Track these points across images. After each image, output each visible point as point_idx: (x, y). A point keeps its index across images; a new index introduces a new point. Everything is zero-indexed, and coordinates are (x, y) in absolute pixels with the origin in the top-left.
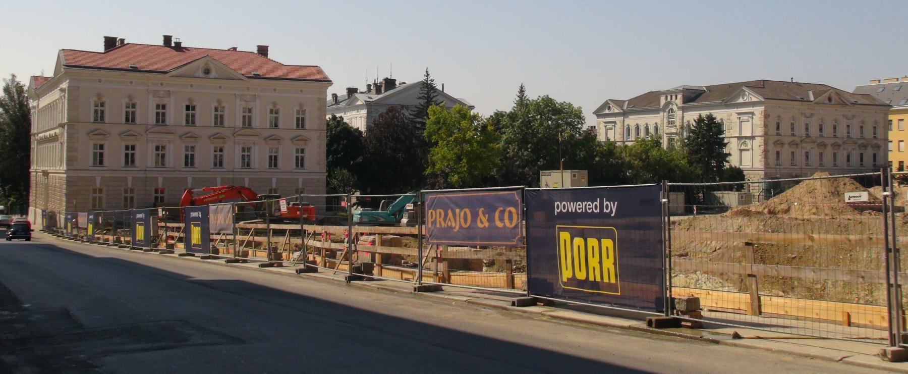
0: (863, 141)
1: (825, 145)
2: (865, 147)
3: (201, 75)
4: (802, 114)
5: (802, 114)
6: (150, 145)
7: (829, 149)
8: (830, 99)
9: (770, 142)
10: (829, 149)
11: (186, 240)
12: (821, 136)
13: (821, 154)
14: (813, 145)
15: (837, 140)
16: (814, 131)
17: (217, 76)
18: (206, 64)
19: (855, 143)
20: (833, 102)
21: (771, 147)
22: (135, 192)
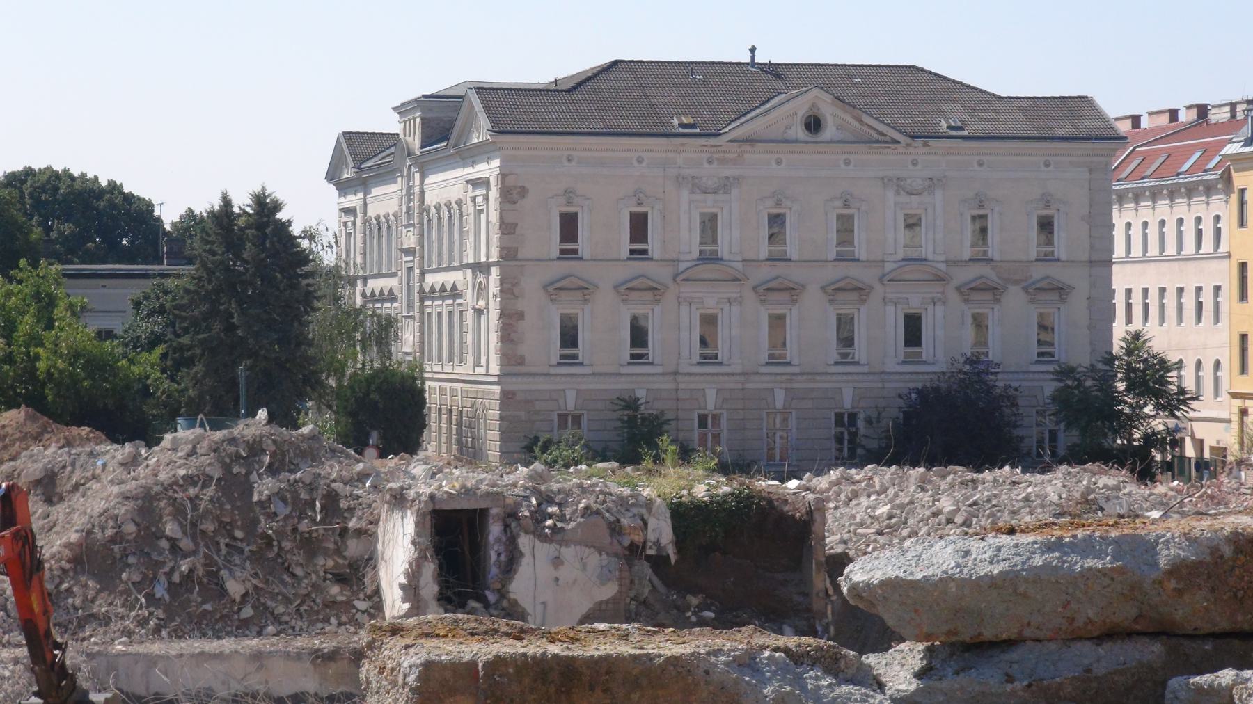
0: (986, 270)
1: (792, 291)
2: (994, 291)
3: (801, 133)
4: (680, 180)
5: (680, 180)
6: (890, 309)
7: (813, 300)
8: (814, 124)
9: (531, 284)
10: (813, 300)
11: (938, 604)
12: (1048, 258)
13: (778, 321)
14: (731, 291)
15: (853, 271)
16: (741, 237)
17: (840, 136)
18: (814, 105)
19: (940, 279)
20: (829, 132)
21: (531, 299)
22: (584, 421)
